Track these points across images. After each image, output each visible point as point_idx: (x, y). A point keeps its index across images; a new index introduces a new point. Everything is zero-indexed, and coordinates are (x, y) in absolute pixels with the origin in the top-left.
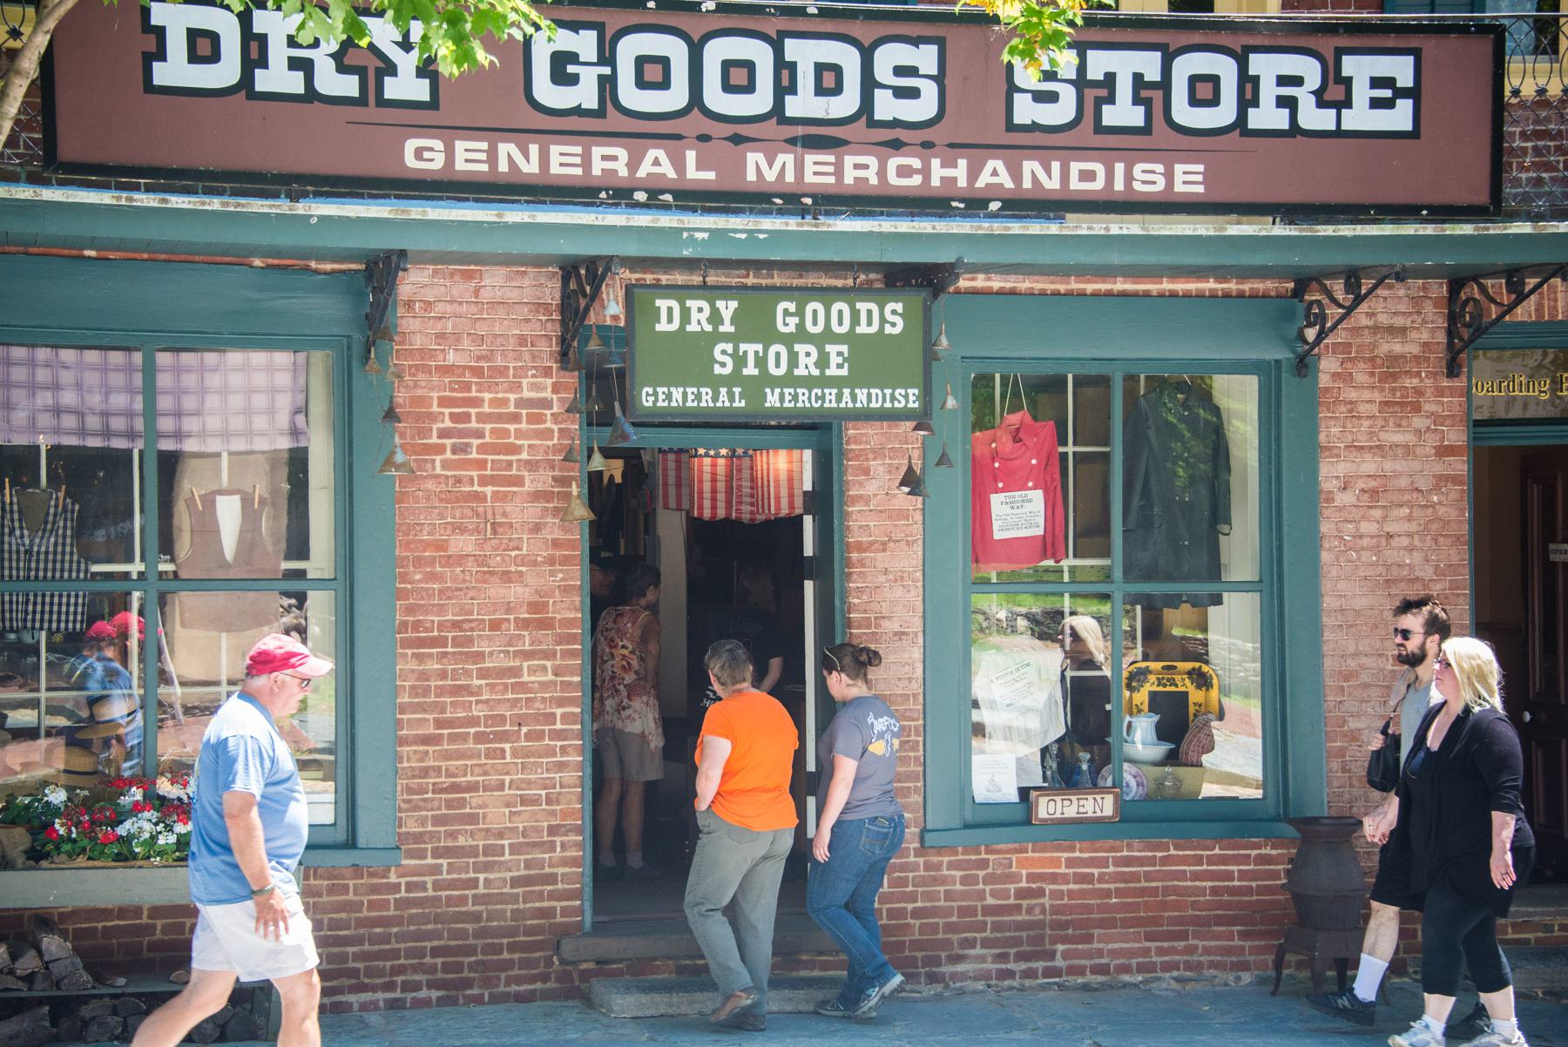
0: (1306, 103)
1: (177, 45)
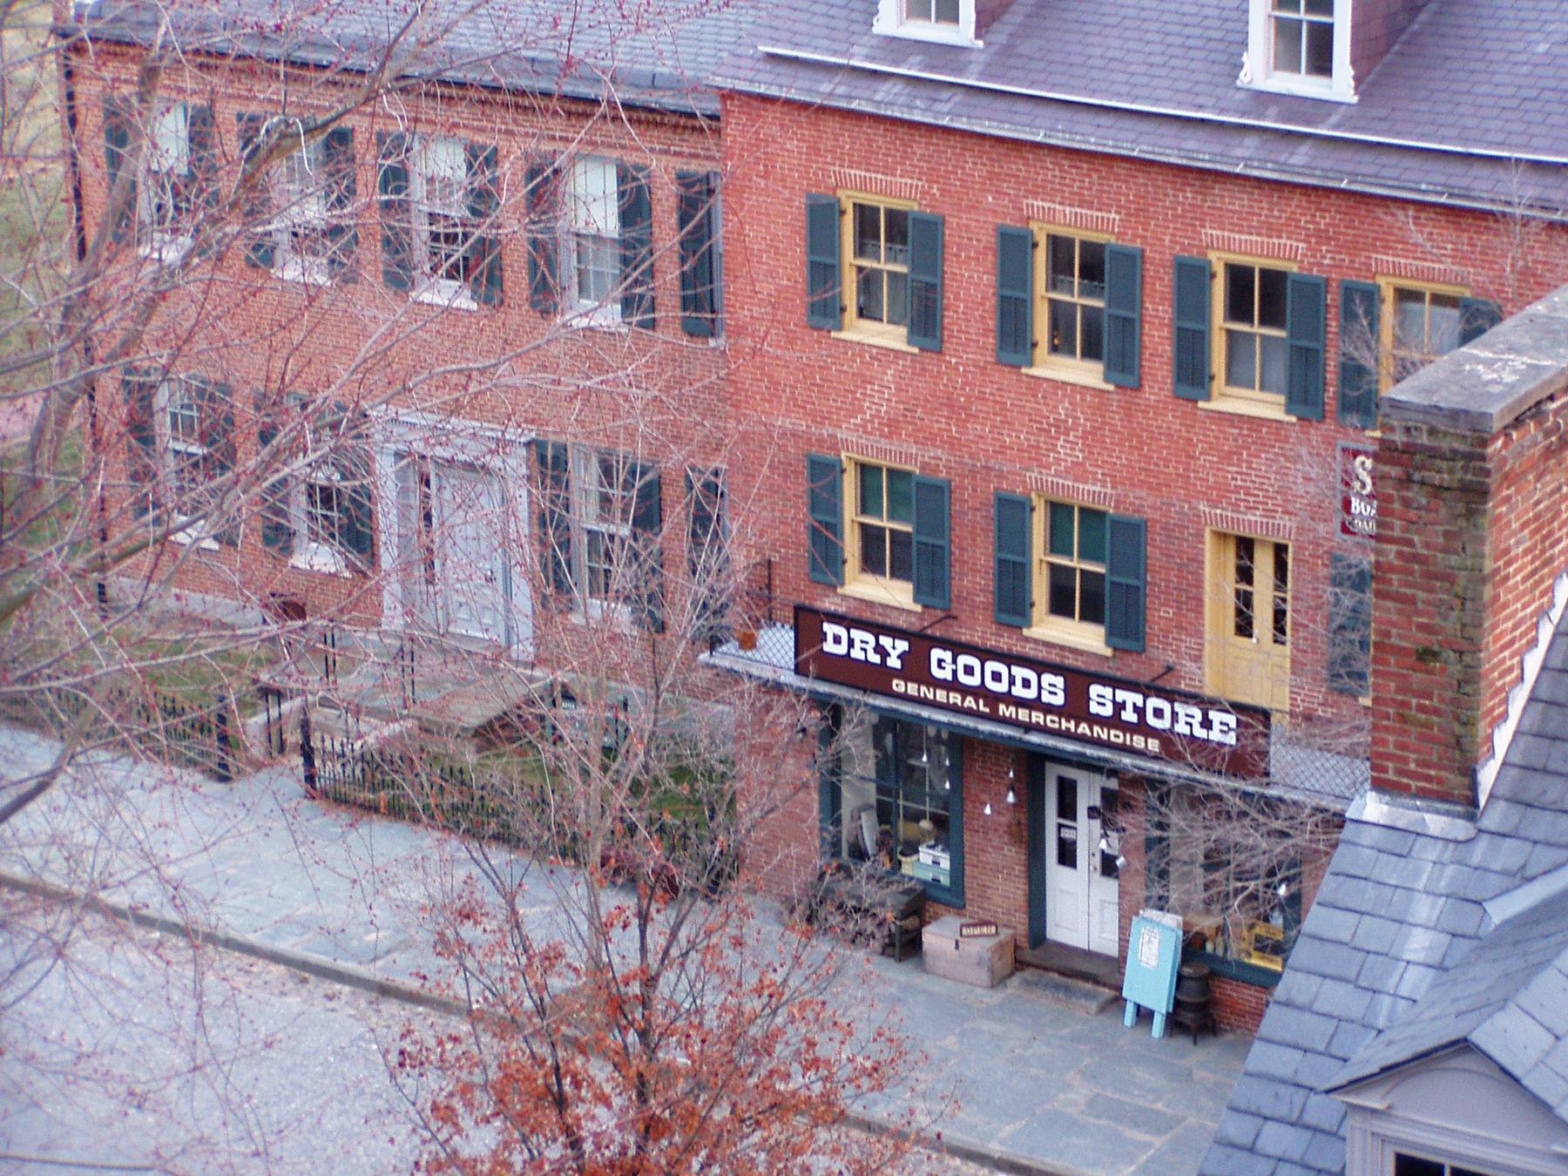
0: (1196, 726)
1: (830, 638)
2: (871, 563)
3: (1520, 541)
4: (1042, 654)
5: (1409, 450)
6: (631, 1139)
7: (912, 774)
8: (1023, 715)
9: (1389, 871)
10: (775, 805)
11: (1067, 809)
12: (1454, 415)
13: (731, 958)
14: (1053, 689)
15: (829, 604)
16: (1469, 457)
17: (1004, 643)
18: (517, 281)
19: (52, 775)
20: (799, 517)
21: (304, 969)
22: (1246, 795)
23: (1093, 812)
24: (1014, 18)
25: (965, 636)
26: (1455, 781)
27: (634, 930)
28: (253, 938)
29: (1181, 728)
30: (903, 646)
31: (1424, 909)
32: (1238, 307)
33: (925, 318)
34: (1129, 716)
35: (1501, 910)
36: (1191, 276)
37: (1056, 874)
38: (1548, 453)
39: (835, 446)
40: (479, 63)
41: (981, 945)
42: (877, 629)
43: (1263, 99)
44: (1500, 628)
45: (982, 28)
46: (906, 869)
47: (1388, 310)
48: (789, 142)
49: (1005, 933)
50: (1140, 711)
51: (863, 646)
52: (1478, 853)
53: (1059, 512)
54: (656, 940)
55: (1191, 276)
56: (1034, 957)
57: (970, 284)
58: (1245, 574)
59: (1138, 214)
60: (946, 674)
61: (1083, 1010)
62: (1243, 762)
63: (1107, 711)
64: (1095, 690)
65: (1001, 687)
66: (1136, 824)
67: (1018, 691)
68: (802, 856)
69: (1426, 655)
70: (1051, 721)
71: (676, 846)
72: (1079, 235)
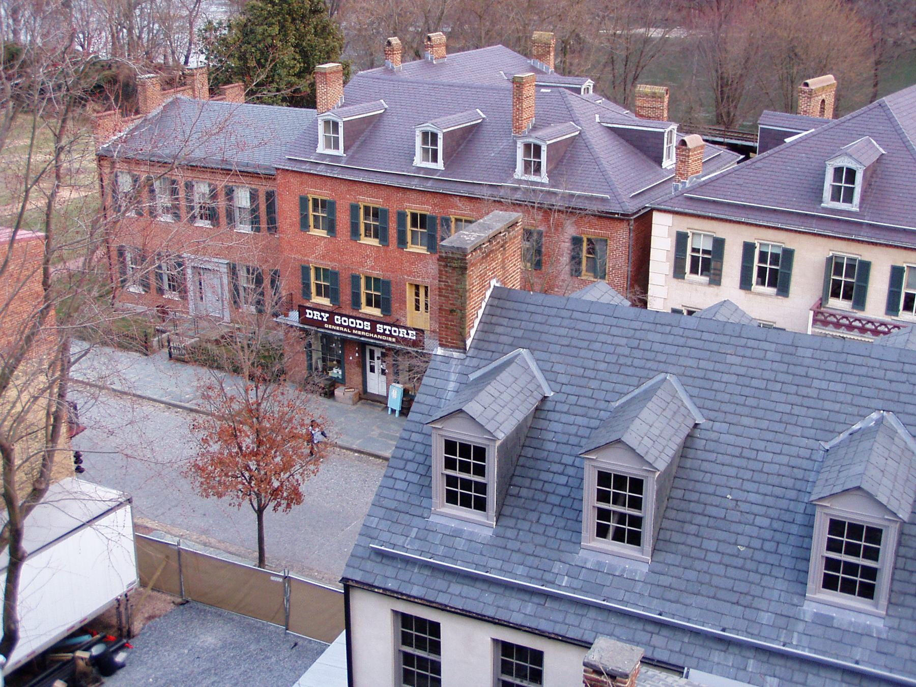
2: (319, 294)
3: (476, 282)
4: (364, 317)
5: (447, 258)
6: (255, 446)
7: (331, 349)
8: (359, 333)
9: (443, 367)
10: (295, 359)
11: (372, 358)
12: (458, 248)
13: (280, 398)
14: (367, 326)
15: (308, 305)
16: (462, 259)
17: (354, 314)
18: (223, 220)
19: (89, 350)
20: (298, 282)
21: (169, 405)
22: (417, 352)
23: (378, 358)
24: (354, 148)
25: (344, 312)
26: (461, 344)
27: (254, 391)
28: (155, 397)
29: (401, 335)
30: (327, 315)
31: (453, 377)
32: (414, 224)
33: (331, 228)
34: (387, 332)
35: (472, 377)
36: (401, 216)
37: (370, 375)
38: (483, 258)
39: (308, 262)
40: (200, 160)
41: (350, 393)
42: (320, 311)
43: (420, 169)
44: (471, 304)
45: (345, 150)
46: (330, 375)
47: (453, 225)
48: (294, 181)
49: (357, 391)
50: (390, 331)
51: (317, 315)
52: (467, 362)
53: (368, 279)
54: (260, 394)
55: (401, 216)
56: (365, 397)
57: (343, 219)
58: (417, 294)
59: (387, 200)
60: (339, 323)
61: (378, 411)
62: (415, 344)
63: (382, 331)
64: (378, 326)
65: (354, 325)
66: (390, 360)
67: (358, 326)
68: (301, 371)
69: (452, 311)
70: (367, 334)
71: (267, 368)
72: (372, 205)
